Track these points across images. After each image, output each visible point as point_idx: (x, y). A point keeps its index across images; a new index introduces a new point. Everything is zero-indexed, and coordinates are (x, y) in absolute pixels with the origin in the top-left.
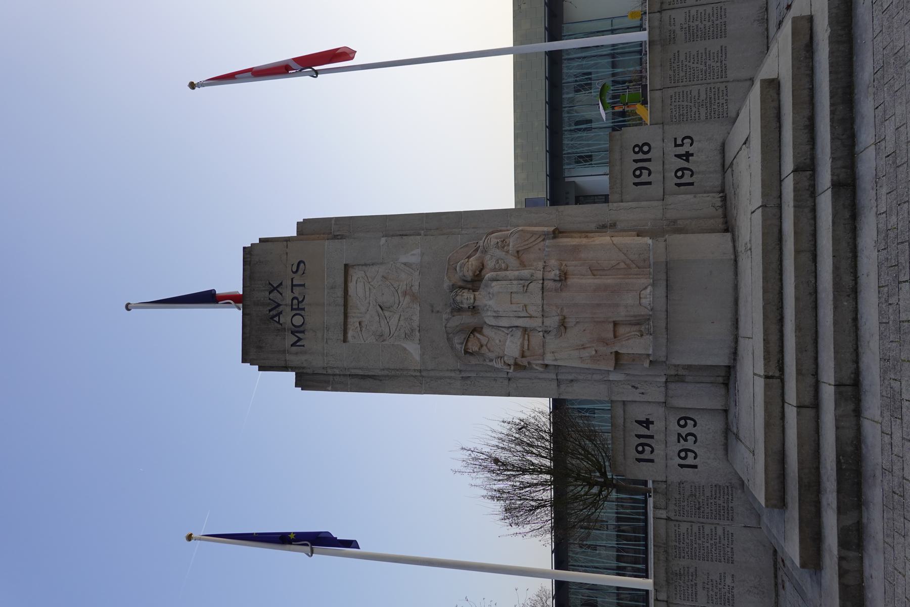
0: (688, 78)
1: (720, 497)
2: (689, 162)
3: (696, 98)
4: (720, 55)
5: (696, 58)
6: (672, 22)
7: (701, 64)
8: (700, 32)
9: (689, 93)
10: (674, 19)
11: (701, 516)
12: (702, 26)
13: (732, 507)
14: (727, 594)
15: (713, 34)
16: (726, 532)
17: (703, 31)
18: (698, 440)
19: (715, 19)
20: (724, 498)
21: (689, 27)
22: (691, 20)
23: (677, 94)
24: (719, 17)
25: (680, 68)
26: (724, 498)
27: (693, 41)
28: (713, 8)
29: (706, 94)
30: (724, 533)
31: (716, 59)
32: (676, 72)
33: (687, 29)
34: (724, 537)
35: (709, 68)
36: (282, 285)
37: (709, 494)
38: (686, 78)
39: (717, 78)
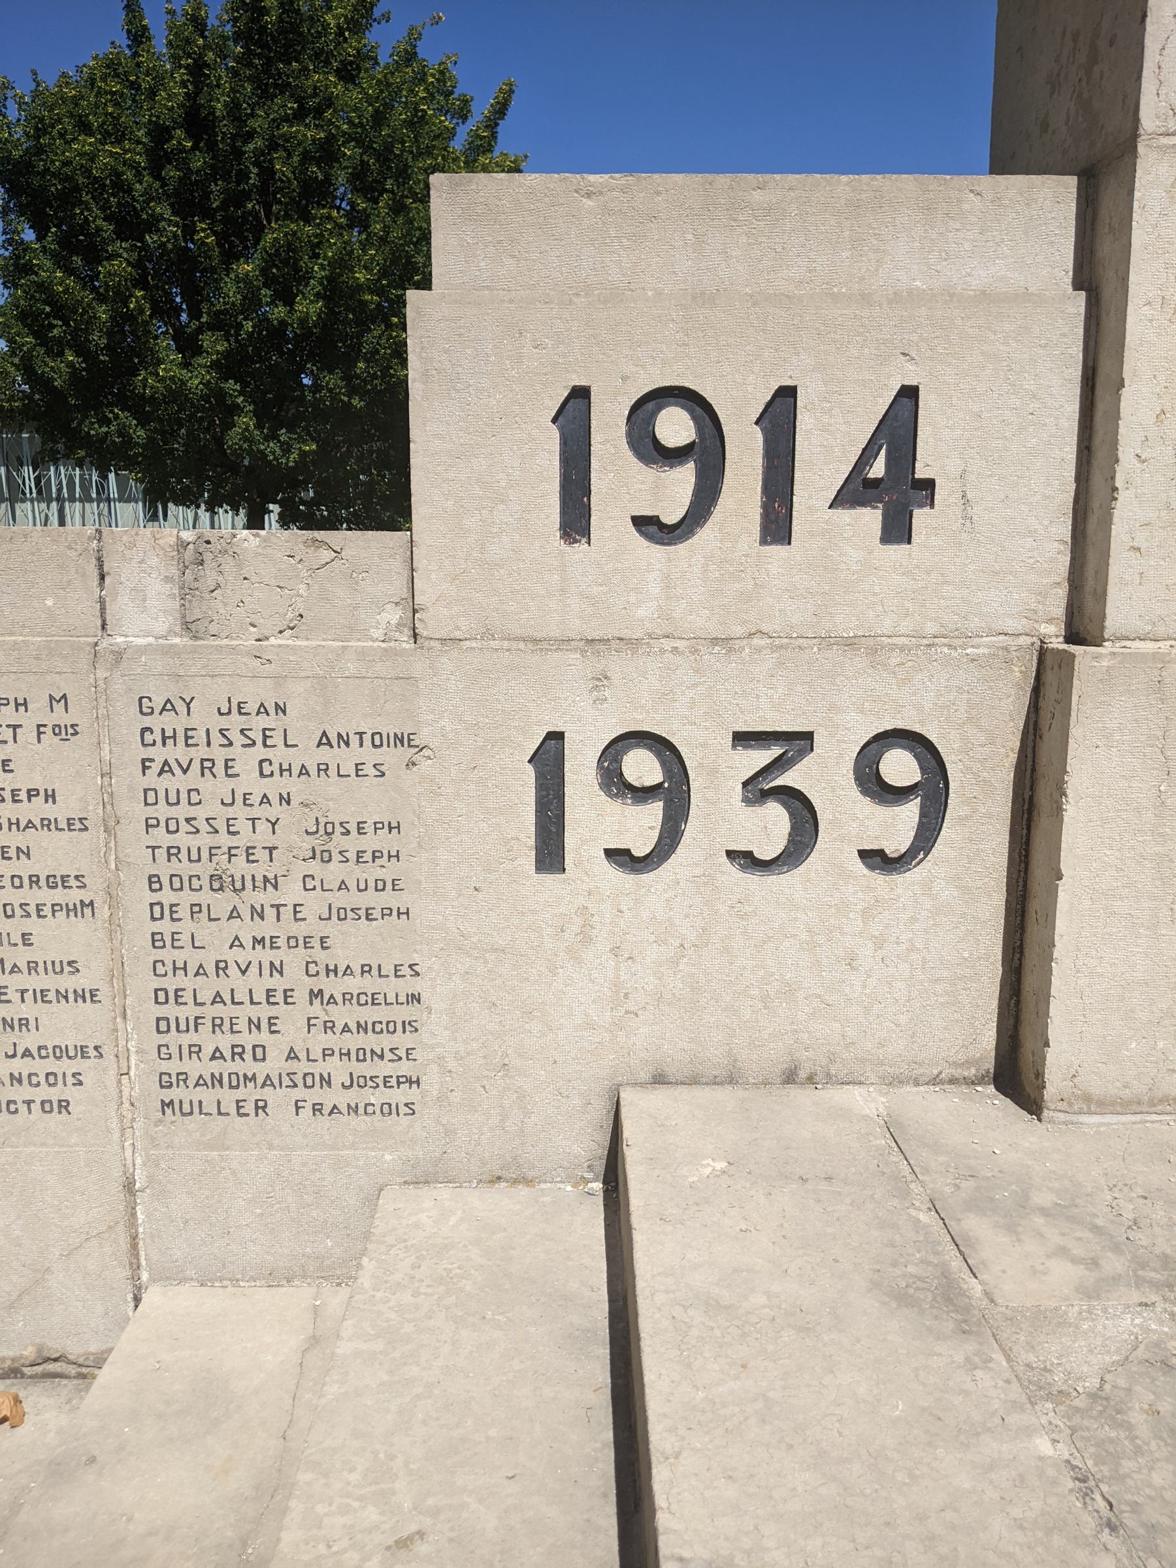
1: (329, 1026)
2: (838, 502)
11: (167, 896)
13: (261, 1107)
14: (215, 787)
16: (66, 1066)
18: (754, 881)
20: (327, 1053)
26: (327, 1053)
30: (60, 1052)
34: (27, 1053)
36: (743, 783)
37: (339, 956)
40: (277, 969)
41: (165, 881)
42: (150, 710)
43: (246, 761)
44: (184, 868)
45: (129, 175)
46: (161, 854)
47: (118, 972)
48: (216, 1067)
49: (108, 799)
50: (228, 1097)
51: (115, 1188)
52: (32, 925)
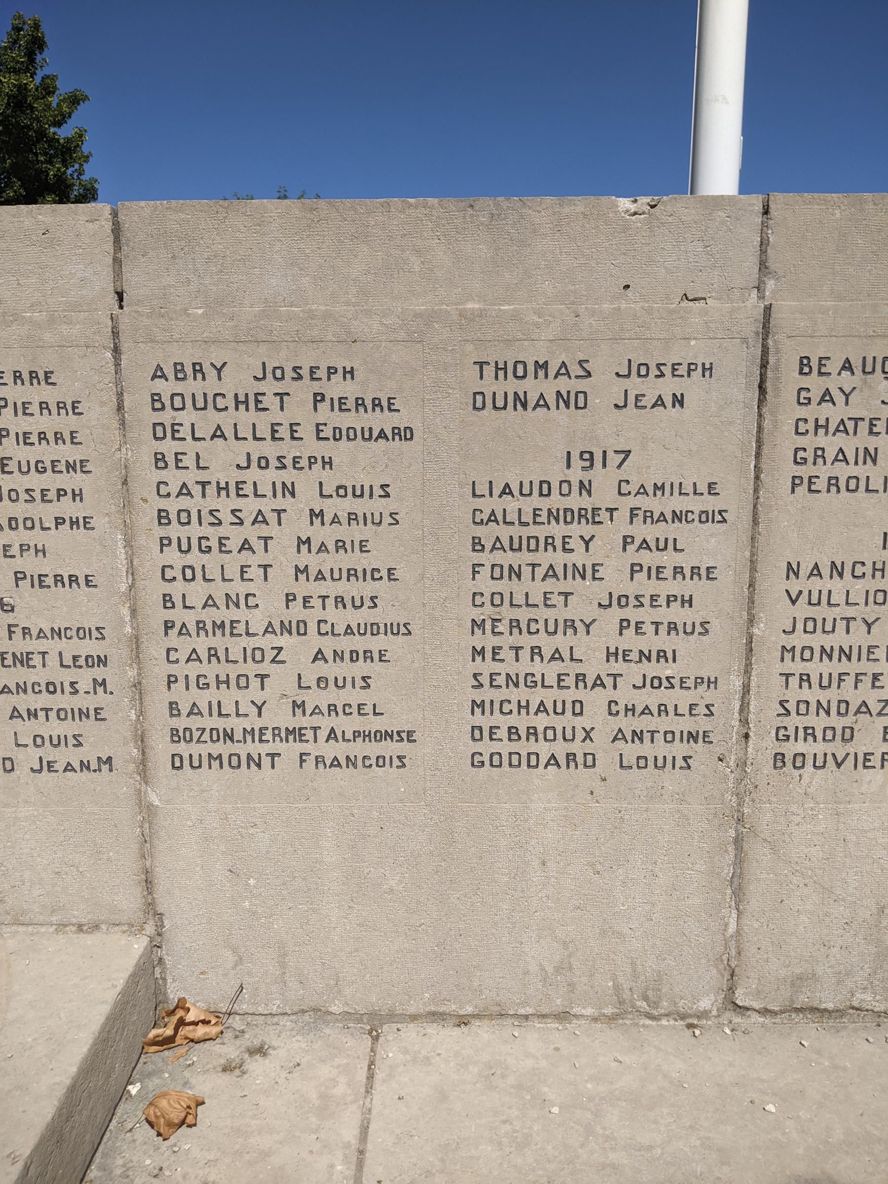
0: (184, 502)
1: (805, 678)
3: (30, 564)
4: (347, 724)
5: (345, 560)
6: (652, 388)
7: (290, 598)
8: (537, 589)
9: (67, 508)
10: (678, 401)
12: (577, 610)
15: (512, 681)
17: (542, 613)
19: (625, 695)
21: (591, 516)
22: (642, 531)
23: (65, 423)
24: (628, 724)
25: (270, 449)
27: (477, 545)
28: (712, 683)
29: (57, 633)
31: (313, 698)
32: (245, 418)
33: (575, 501)
35: (255, 655)
38: (184, 491)
39: (173, 708)
41: (173, 516)
42: (806, 401)
46: (794, 682)
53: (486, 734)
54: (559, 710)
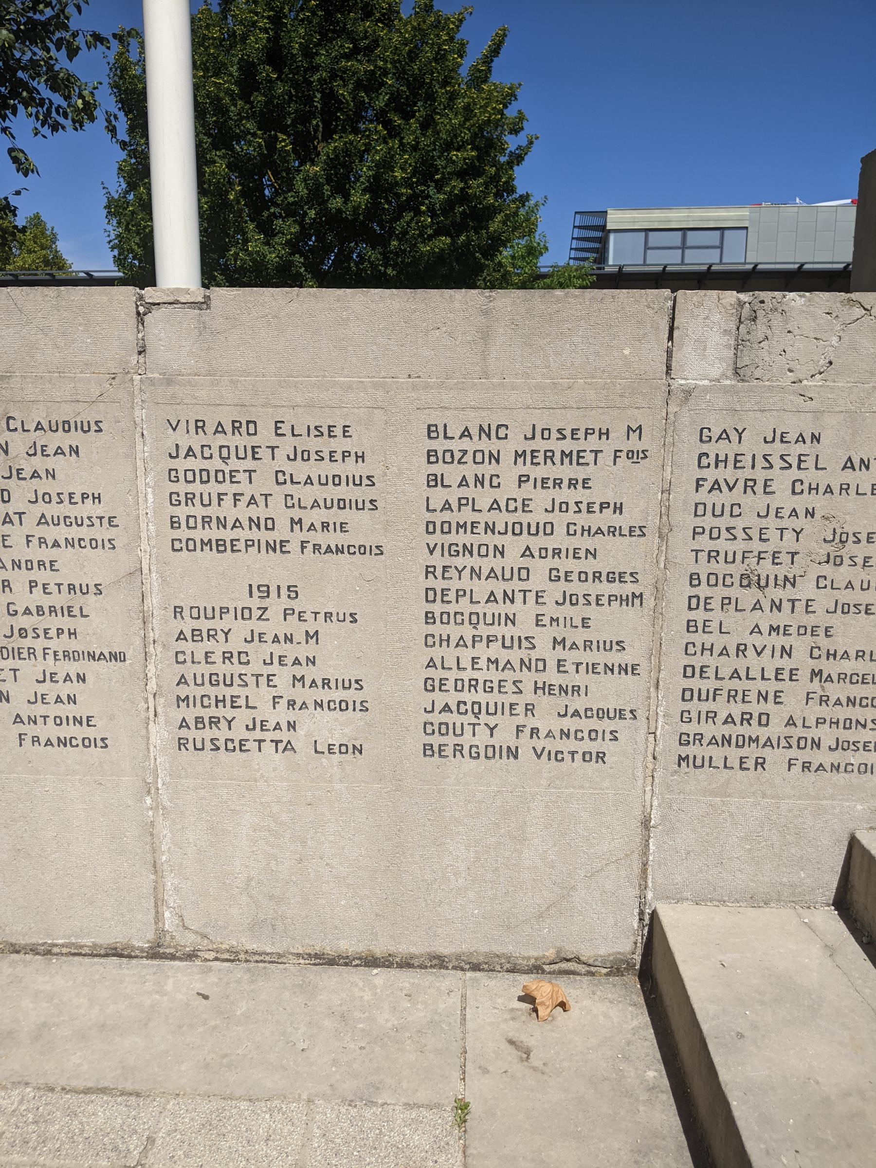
1: (824, 700)
11: (703, 591)
13: (760, 763)
14: (759, 502)
16: (607, 725)
30: (602, 714)
40: (786, 652)
43: (782, 481)
44: (721, 568)
45: (227, 100)
47: (657, 651)
48: (727, 730)
49: (666, 511)
50: (734, 754)
51: (635, 824)
52: (592, 612)
53: (809, 631)
54: (56, 522)
